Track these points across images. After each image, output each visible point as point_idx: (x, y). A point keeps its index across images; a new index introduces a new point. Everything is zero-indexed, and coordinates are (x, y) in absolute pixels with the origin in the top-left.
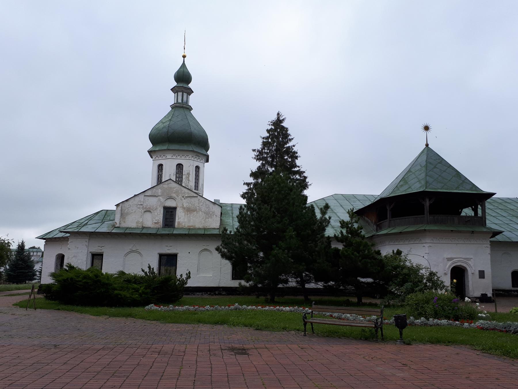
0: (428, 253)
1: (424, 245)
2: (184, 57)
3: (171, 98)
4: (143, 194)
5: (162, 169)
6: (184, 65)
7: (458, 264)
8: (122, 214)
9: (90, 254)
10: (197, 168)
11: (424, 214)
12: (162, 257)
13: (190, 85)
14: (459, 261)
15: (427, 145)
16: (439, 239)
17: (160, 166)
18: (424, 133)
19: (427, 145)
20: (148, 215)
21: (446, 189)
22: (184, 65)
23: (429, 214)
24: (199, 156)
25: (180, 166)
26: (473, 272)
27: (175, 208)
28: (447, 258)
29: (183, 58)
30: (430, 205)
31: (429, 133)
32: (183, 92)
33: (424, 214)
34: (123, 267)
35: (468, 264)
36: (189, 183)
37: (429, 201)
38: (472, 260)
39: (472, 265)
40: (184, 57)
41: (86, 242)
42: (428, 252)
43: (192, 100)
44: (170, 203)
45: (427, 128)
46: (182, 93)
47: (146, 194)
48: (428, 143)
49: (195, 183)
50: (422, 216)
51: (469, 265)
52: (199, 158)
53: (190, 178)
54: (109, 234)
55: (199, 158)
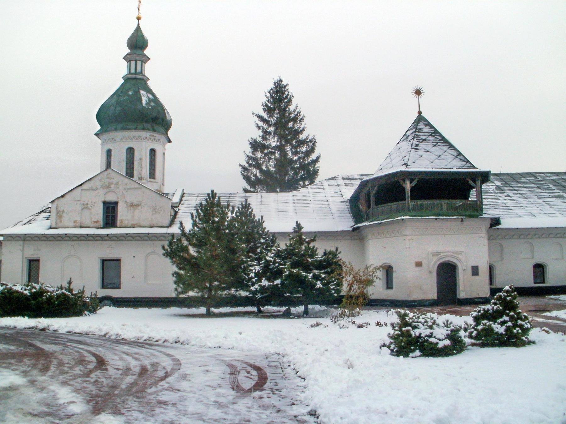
0: (409, 248)
1: (404, 237)
2: (139, 19)
3: (123, 69)
4: (80, 188)
5: (154, 155)
6: (138, 29)
7: (446, 259)
8: (58, 212)
9: (26, 260)
10: (153, 152)
11: (405, 200)
12: (32, 262)
13: (146, 52)
14: (447, 256)
15: (420, 113)
16: (415, 230)
17: (109, 152)
18: (415, 99)
19: (420, 113)
20: (86, 213)
21: (425, 168)
22: (138, 29)
23: (411, 200)
24: (157, 138)
25: (130, 151)
26: (464, 268)
27: (116, 203)
28: (431, 253)
29: (138, 21)
30: (412, 189)
31: (422, 98)
32: (136, 61)
33: (405, 200)
34: (528, 281)
35: (458, 259)
36: (141, 170)
37: (411, 183)
38: (463, 254)
39: (463, 260)
40: (139, 19)
41: (20, 245)
42: (409, 247)
43: (149, 70)
44: (111, 198)
45: (418, 92)
46: (462, 294)
47: (84, 187)
48: (421, 110)
49: (150, 169)
50: (404, 202)
51: (460, 260)
52: (150, 138)
53: (144, 165)
54: (538, 230)
55: (155, 138)
